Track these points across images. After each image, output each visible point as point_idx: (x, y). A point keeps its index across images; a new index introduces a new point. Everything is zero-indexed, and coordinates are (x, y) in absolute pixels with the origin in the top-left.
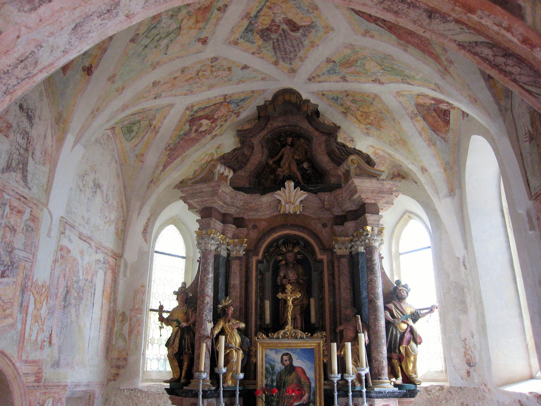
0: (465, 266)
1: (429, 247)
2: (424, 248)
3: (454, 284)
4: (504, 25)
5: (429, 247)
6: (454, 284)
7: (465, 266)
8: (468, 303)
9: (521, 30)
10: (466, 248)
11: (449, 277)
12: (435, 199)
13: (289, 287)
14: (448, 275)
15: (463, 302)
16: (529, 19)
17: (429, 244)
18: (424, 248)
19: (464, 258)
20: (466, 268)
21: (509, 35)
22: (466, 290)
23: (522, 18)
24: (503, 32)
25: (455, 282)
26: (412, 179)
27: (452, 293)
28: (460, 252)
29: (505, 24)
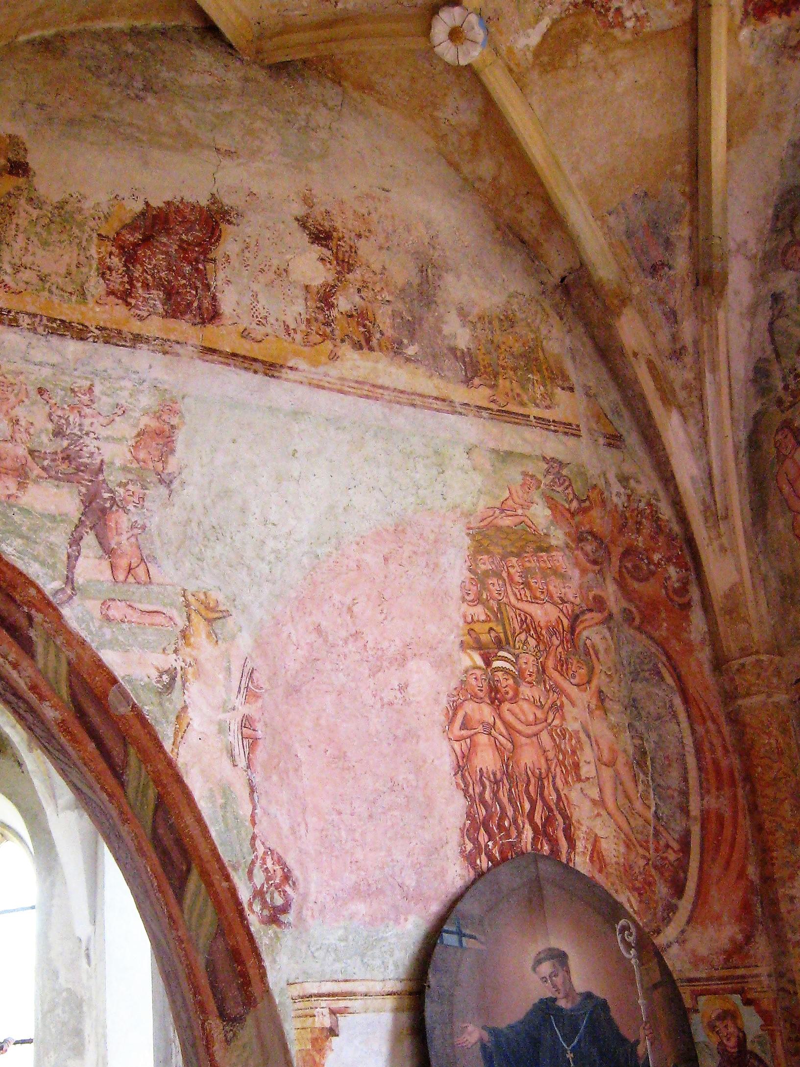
0: (88, 956)
1: (33, 908)
2: (23, 909)
3: (65, 994)
4: (10, 659)
5: (33, 908)
6: (65, 994)
7: (88, 956)
8: (86, 1034)
9: (30, 672)
10: (94, 921)
11: (57, 978)
12: (49, 810)
13: (717, 1024)
14: (56, 974)
15: (78, 1033)
16: (40, 658)
17: (34, 902)
18: (23, 909)
19: (89, 940)
20: (89, 963)
21: (14, 674)
22: (85, 1009)
23: (33, 657)
24: (8, 667)
25: (68, 990)
26: (14, 755)
27: (59, 1011)
28: (83, 929)
29: (12, 657)
